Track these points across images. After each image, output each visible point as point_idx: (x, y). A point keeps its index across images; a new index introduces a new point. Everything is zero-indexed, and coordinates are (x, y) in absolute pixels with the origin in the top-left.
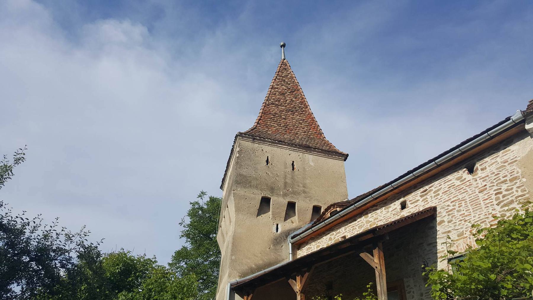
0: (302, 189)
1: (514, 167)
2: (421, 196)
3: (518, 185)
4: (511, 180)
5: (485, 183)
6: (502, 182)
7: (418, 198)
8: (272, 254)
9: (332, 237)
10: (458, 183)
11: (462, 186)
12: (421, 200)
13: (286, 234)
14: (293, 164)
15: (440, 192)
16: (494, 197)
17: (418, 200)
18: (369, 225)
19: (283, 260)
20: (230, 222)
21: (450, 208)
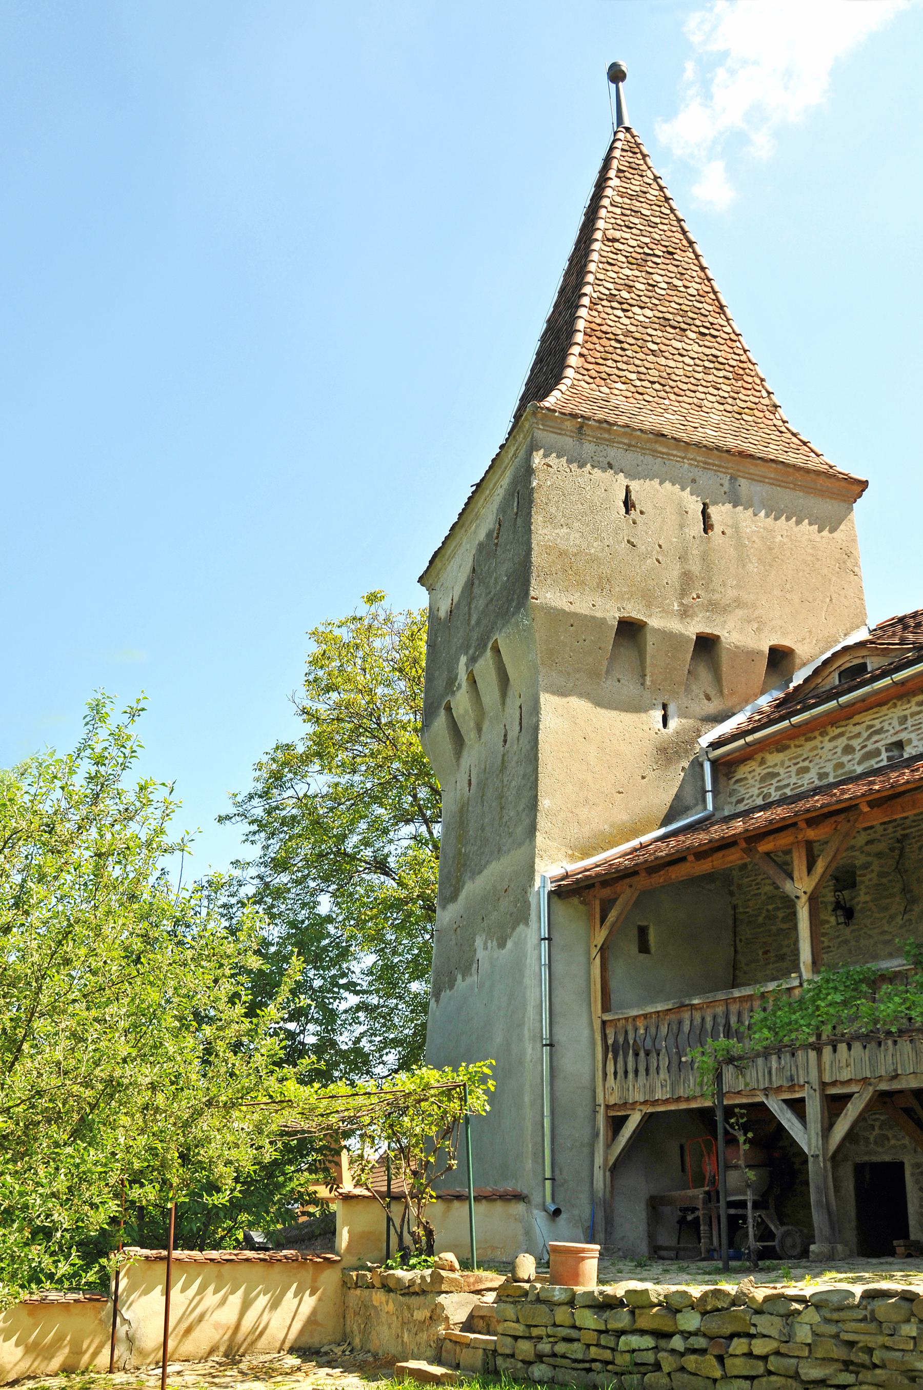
9: (856, 743)
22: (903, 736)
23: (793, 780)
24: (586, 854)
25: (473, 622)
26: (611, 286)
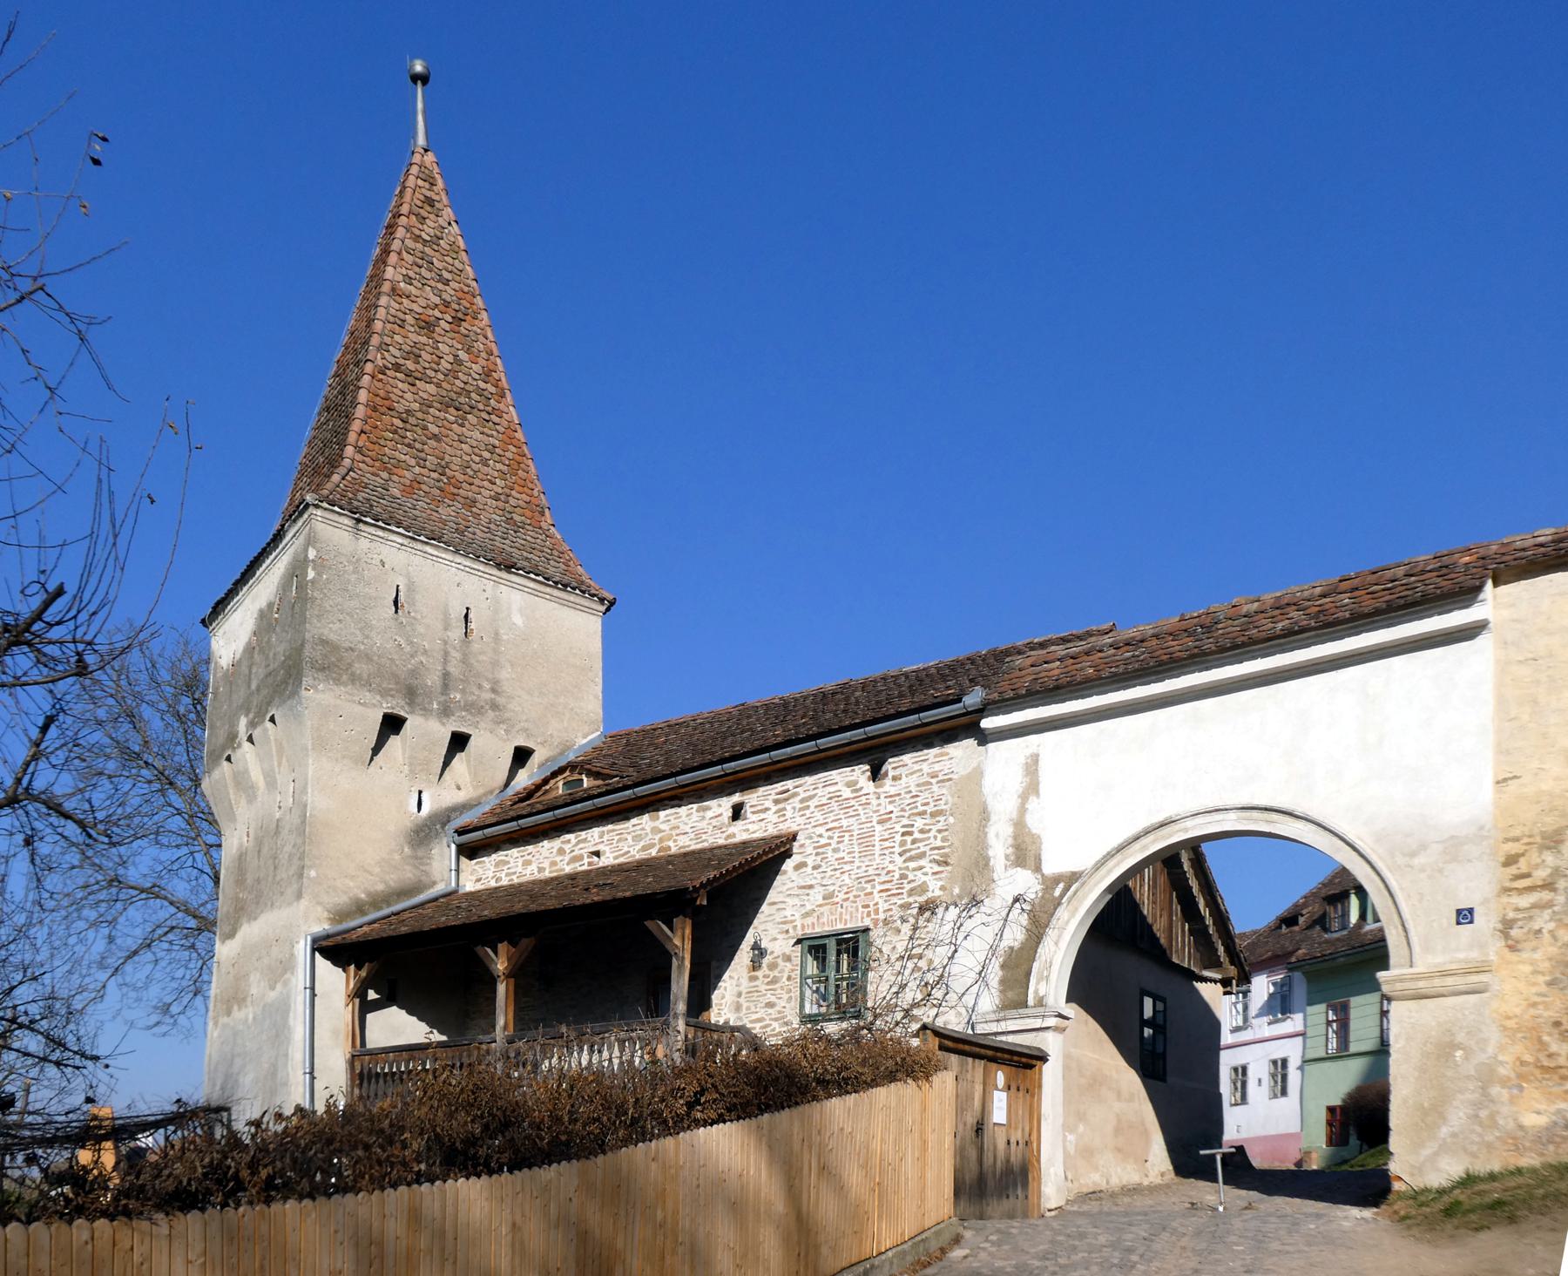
0: (488, 696)
1: (944, 791)
2: (776, 802)
3: (939, 826)
4: (933, 815)
5: (890, 808)
6: (919, 814)
7: (768, 804)
8: (408, 868)
9: (567, 847)
10: (847, 793)
11: (853, 802)
12: (774, 809)
13: (442, 818)
14: (466, 616)
15: (812, 803)
16: (898, 838)
17: (767, 809)
18: (657, 837)
19: (434, 883)
20: (94, 613)
21: (823, 841)
22: (600, 847)
23: (519, 869)
24: (340, 922)
25: (254, 687)
26: (397, 353)
